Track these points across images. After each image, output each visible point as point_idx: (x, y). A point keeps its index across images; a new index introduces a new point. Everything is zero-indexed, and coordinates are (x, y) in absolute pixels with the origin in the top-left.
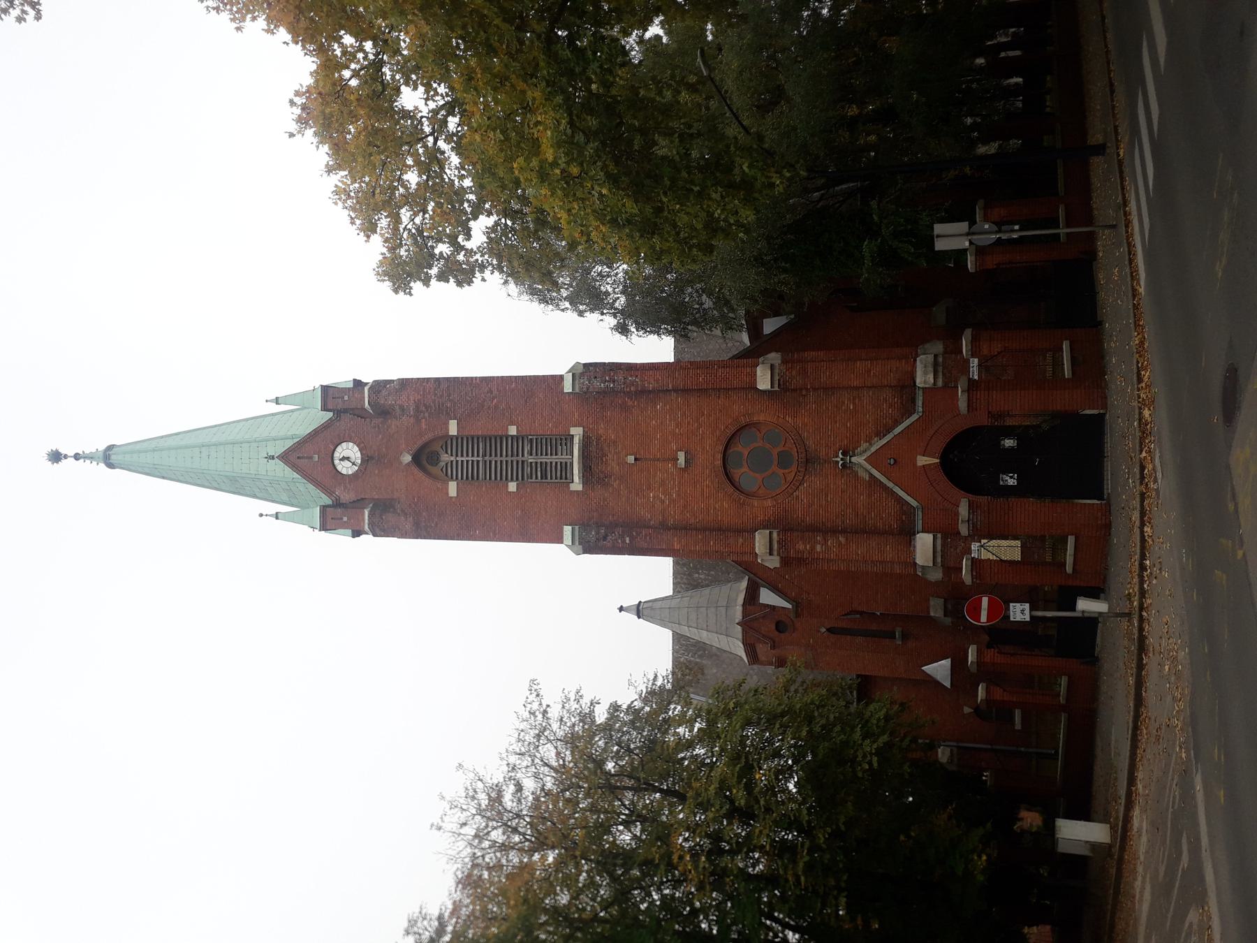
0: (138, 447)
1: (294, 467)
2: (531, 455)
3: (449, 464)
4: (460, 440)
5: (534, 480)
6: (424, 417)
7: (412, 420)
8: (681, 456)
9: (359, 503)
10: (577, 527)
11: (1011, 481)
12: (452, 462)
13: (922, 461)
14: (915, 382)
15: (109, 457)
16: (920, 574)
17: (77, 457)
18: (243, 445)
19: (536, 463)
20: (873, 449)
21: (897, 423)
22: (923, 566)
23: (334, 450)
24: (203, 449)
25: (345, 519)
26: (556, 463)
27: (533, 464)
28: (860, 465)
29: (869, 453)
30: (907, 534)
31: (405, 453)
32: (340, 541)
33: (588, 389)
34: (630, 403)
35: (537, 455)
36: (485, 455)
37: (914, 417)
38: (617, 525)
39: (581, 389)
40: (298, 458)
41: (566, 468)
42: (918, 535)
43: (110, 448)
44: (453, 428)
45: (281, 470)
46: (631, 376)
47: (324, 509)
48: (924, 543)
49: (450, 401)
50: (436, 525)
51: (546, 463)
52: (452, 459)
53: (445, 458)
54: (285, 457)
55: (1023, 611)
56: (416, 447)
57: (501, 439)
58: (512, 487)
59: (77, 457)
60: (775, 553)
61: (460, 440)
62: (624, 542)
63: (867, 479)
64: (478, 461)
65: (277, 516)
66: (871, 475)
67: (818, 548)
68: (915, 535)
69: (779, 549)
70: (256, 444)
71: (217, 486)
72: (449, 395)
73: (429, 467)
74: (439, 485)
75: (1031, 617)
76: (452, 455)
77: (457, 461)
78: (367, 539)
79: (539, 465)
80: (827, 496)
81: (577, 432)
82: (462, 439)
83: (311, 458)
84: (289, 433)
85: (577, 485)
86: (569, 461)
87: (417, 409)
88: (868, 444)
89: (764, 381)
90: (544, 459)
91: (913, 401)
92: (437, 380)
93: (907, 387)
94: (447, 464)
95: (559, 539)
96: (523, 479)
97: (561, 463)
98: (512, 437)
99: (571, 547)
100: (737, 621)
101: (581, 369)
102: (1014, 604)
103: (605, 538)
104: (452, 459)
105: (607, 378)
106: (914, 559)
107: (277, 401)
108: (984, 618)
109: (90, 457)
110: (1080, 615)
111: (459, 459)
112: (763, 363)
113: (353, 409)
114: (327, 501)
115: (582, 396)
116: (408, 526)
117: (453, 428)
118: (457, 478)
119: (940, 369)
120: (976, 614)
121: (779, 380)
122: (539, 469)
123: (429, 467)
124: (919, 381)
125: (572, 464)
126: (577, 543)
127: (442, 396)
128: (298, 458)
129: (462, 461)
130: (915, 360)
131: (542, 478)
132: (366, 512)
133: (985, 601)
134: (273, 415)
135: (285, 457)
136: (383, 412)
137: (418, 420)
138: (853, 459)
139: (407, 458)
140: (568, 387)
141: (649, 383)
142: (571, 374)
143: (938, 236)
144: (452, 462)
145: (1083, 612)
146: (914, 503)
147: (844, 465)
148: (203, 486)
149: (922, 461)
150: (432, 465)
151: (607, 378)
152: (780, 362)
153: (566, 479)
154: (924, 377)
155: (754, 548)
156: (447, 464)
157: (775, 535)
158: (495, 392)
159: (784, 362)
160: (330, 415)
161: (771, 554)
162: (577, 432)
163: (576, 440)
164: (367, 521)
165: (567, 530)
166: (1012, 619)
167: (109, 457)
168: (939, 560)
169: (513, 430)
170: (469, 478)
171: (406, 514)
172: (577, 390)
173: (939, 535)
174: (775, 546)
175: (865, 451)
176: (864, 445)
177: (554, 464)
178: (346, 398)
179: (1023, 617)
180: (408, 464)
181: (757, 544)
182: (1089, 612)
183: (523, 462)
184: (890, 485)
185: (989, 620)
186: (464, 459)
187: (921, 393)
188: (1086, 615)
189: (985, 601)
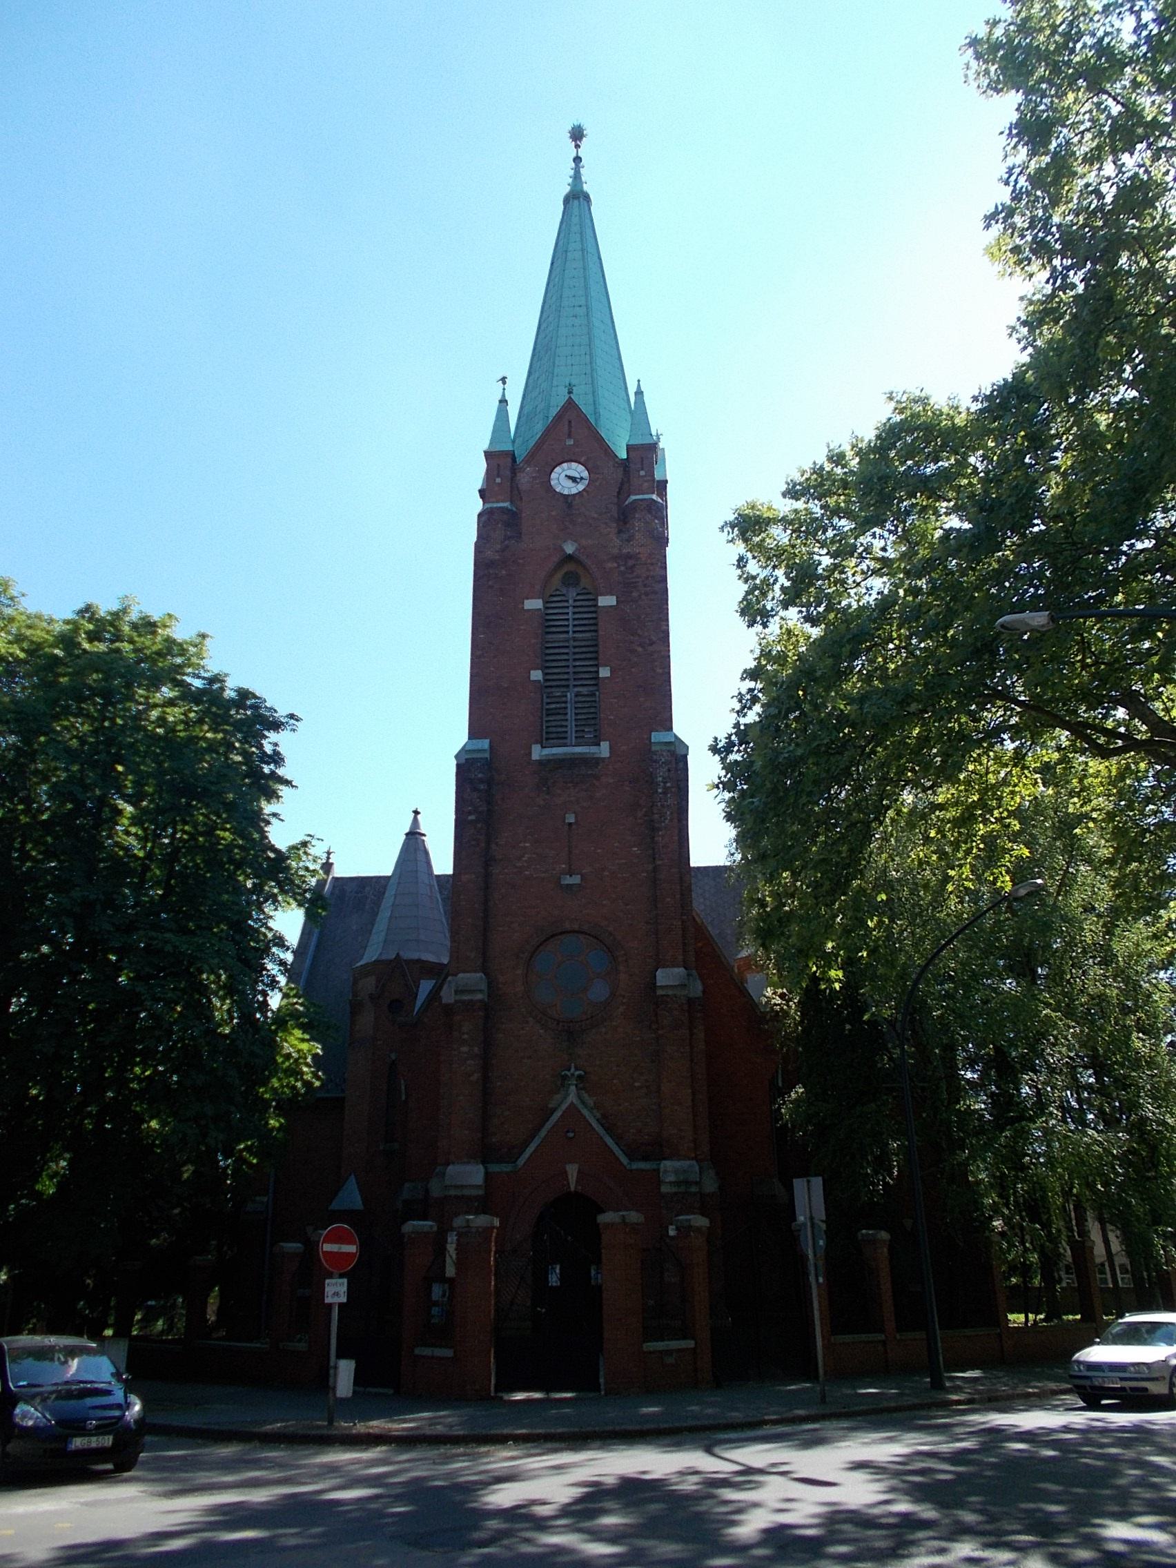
0: (589, 231)
1: (559, 417)
2: (576, 696)
3: (563, 598)
4: (593, 609)
5: (546, 700)
6: (619, 566)
7: (616, 551)
8: (576, 880)
9: (514, 492)
10: (487, 755)
11: (554, 1280)
12: (567, 601)
13: (572, 1170)
14: (665, 1159)
15: (577, 199)
16: (437, 1170)
17: (577, 160)
18: (588, 357)
19: (566, 702)
20: (585, 1112)
21: (618, 1139)
22: (444, 1174)
23: (580, 463)
24: (584, 309)
25: (498, 480)
26: (566, 726)
27: (564, 699)
28: (567, 1095)
29: (580, 1106)
30: (485, 1153)
31: (576, 545)
32: (478, 470)
33: (656, 761)
34: (640, 814)
35: (576, 702)
36: (575, 640)
37: (624, 1160)
38: (489, 803)
39: (655, 753)
40: (570, 422)
41: (561, 739)
42: (481, 1166)
43: (587, 198)
44: (607, 601)
45: (559, 400)
46: (671, 813)
47: (512, 455)
48: (472, 1175)
49: (640, 596)
50: (491, 587)
51: (566, 714)
52: (571, 602)
53: (572, 594)
54: (570, 405)
55: (336, 1294)
56: (583, 558)
57: (596, 659)
58: (537, 675)
59: (577, 160)
60: (458, 997)
61: (593, 609)
62: (470, 813)
63: (550, 1106)
64: (568, 632)
65: (503, 401)
66: (554, 1110)
67: (465, 1049)
68: (483, 1163)
69: (463, 1002)
70: (588, 371)
71: (542, 328)
72: (646, 594)
73: (559, 575)
74: (538, 587)
75: (330, 1305)
76: (575, 601)
77: (568, 607)
78: (478, 505)
79: (563, 705)
80: (530, 1057)
81: (604, 750)
82: (595, 612)
83: (570, 436)
84: (602, 411)
85: (537, 753)
86: (568, 741)
87: (629, 556)
88: (592, 1105)
89: (667, 977)
90: (570, 715)
91: (645, 1158)
92: (664, 579)
93: (656, 1149)
94: (563, 595)
95: (473, 734)
96: (546, 687)
97: (566, 732)
98: (597, 672)
99: (464, 750)
100: (401, 953)
101: (680, 752)
102: (346, 1284)
103: (475, 789)
104: (571, 602)
105: (668, 785)
106: (453, 1163)
107: (639, 393)
108: (328, 1247)
109: (577, 176)
110: (332, 1364)
111: (570, 610)
112: (688, 975)
113: (629, 481)
114: (521, 454)
115: (646, 753)
116: (489, 554)
117: (607, 601)
118: (547, 608)
119: (682, 1189)
120: (336, 1238)
121: (668, 996)
122: (558, 706)
123: (559, 575)
124: (667, 1164)
125: (565, 745)
126: (467, 757)
127: (645, 586)
128: (570, 422)
129: (568, 613)
130: (692, 1159)
131: (547, 710)
132: (506, 505)
133: (352, 1249)
134: (626, 388)
135: (570, 405)
136: (624, 517)
137: (615, 558)
138: (573, 1088)
139: (570, 548)
140: (657, 737)
141: (663, 836)
142: (673, 740)
143: (808, 1182)
144: (567, 601)
145: (336, 1368)
146: (521, 1161)
147: (565, 1078)
148: (542, 312)
149: (572, 1170)
150: (563, 577)
151: (668, 785)
152: (691, 995)
153: (547, 739)
154: (670, 1169)
155: (464, 971)
156: (563, 595)
157: (479, 996)
158: (651, 649)
159: (690, 1001)
160: (623, 455)
161: (456, 992)
162: (604, 750)
163: (593, 749)
164: (495, 505)
165: (485, 744)
166: (327, 1281)
167: (577, 199)
168: (452, 1192)
169: (604, 672)
170: (546, 622)
171: (503, 550)
172: (653, 748)
173: (481, 1192)
174: (466, 997)
175: (583, 1103)
176: (590, 1101)
177: (564, 723)
178: (642, 473)
179: (330, 1294)
180: (564, 550)
181: (468, 975)
182: (335, 1375)
183: (568, 686)
184: (543, 1133)
185: (326, 1253)
186: (570, 616)
187: (655, 1167)
188: (332, 1372)
189: (352, 1249)
